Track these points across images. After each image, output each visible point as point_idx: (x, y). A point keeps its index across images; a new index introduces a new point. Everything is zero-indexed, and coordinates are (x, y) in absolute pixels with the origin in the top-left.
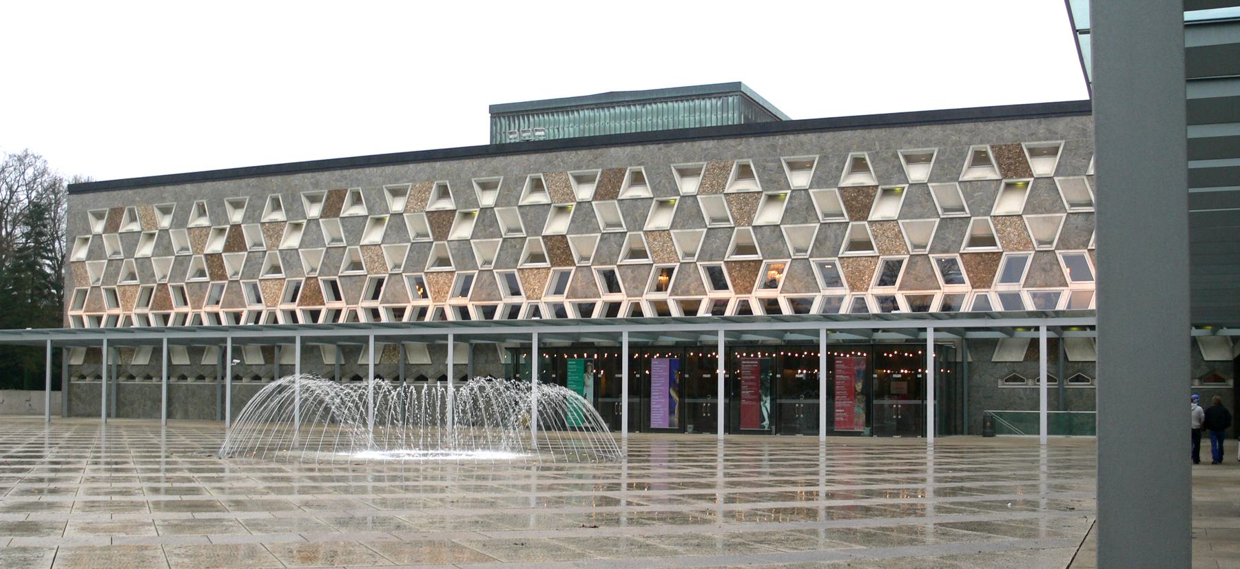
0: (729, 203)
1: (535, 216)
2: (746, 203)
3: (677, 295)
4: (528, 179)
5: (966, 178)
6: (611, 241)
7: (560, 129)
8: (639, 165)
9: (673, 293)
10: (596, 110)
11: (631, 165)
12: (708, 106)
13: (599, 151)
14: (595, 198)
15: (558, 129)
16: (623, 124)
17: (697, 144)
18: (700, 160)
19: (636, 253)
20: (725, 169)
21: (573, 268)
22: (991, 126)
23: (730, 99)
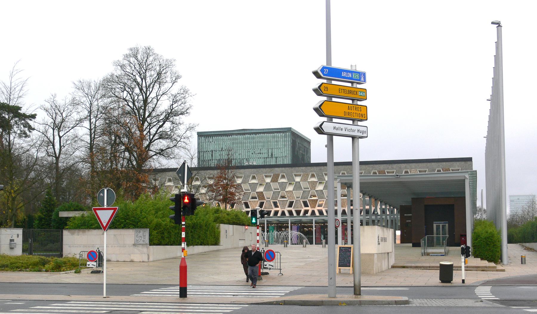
0: (309, 184)
1: (254, 186)
2: (314, 184)
3: (295, 208)
4: (251, 176)
5: (250, 182)
6: (276, 194)
7: (225, 142)
8: (284, 173)
9: (294, 208)
10: (238, 136)
11: (281, 173)
12: (280, 135)
13: (272, 169)
14: (271, 182)
15: (224, 142)
16: (248, 141)
17: (300, 168)
18: (301, 172)
19: (283, 197)
20: (308, 175)
21: (265, 201)
22: (377, 166)
23: (287, 133)
